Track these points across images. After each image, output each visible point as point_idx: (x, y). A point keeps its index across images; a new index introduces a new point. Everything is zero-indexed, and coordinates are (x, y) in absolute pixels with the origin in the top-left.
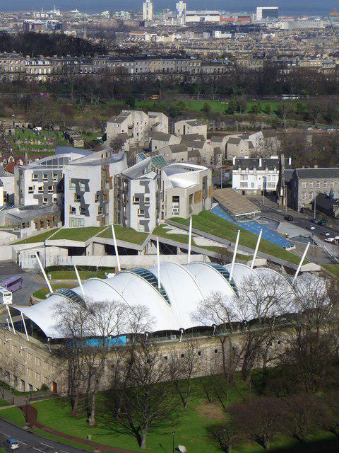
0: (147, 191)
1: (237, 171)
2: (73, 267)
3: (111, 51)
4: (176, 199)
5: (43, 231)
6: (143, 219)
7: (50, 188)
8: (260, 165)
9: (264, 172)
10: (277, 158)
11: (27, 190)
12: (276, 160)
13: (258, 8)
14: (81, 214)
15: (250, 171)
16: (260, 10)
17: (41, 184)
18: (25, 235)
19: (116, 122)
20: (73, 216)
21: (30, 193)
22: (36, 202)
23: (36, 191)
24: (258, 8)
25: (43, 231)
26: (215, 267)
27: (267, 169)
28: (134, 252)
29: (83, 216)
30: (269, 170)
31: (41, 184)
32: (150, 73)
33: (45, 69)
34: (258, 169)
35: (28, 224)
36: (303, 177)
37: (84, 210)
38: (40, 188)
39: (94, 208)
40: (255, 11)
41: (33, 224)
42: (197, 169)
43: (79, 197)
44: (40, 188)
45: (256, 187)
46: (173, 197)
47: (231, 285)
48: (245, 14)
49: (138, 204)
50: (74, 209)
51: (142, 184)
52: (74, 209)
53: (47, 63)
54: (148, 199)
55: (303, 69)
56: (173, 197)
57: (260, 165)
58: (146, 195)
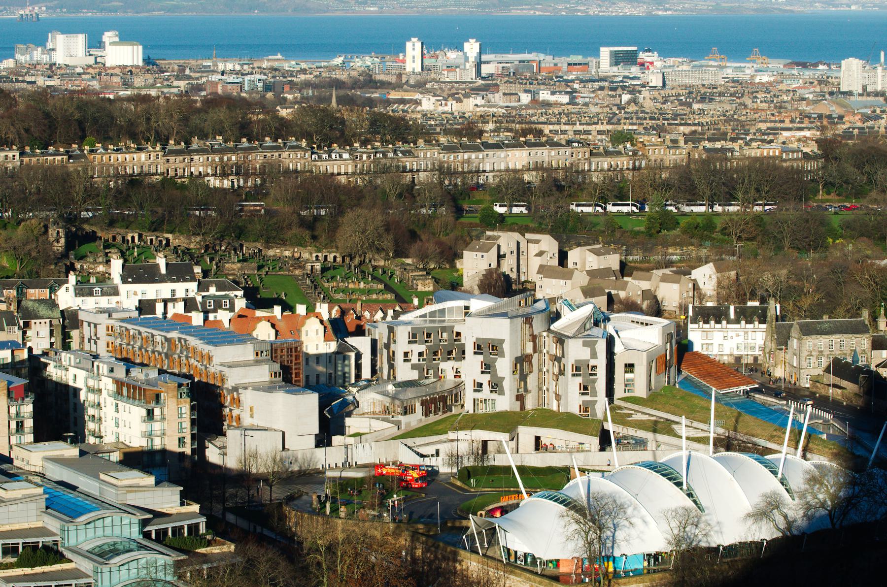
0: (594, 355)
1: (696, 326)
2: (508, 469)
3: (487, 132)
4: (630, 367)
5: (433, 418)
6: (587, 398)
7: (435, 354)
8: (732, 316)
9: (738, 326)
10: (756, 304)
11: (399, 357)
12: (756, 307)
13: (602, 49)
14: (491, 392)
15: (748, 326)
16: (605, 52)
17: (423, 348)
18: (408, 424)
19: (479, 250)
20: (479, 396)
21: (405, 361)
22: (414, 375)
23: (415, 359)
24: (602, 49)
25: (433, 418)
26: (756, 459)
27: (743, 322)
28: (61, 483)
29: (494, 396)
30: (746, 323)
31: (423, 348)
32: (515, 171)
33: (335, 167)
34: (728, 323)
35: (413, 411)
36: (32, 352)
37: (496, 386)
38: (421, 354)
39: (509, 384)
40: (597, 54)
41: (419, 408)
42: (657, 323)
43: (488, 368)
44: (421, 354)
45: (727, 351)
46: (626, 365)
47: (782, 483)
48: (578, 59)
49: (580, 375)
50: (480, 385)
51: (585, 344)
52: (480, 385)
53: (346, 156)
54: (594, 367)
55: (756, 159)
56: (626, 365)
57: (732, 316)
58: (592, 363)
